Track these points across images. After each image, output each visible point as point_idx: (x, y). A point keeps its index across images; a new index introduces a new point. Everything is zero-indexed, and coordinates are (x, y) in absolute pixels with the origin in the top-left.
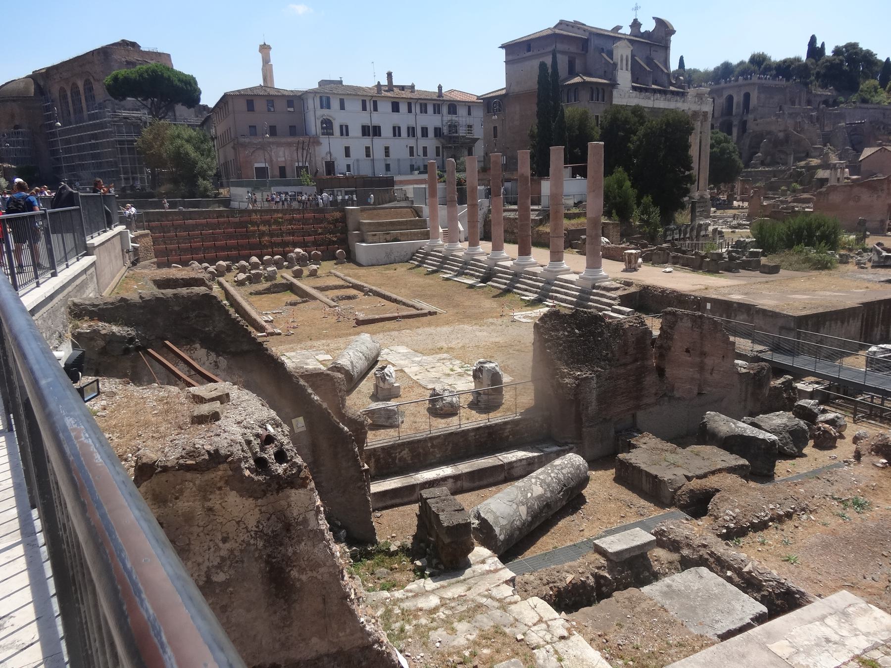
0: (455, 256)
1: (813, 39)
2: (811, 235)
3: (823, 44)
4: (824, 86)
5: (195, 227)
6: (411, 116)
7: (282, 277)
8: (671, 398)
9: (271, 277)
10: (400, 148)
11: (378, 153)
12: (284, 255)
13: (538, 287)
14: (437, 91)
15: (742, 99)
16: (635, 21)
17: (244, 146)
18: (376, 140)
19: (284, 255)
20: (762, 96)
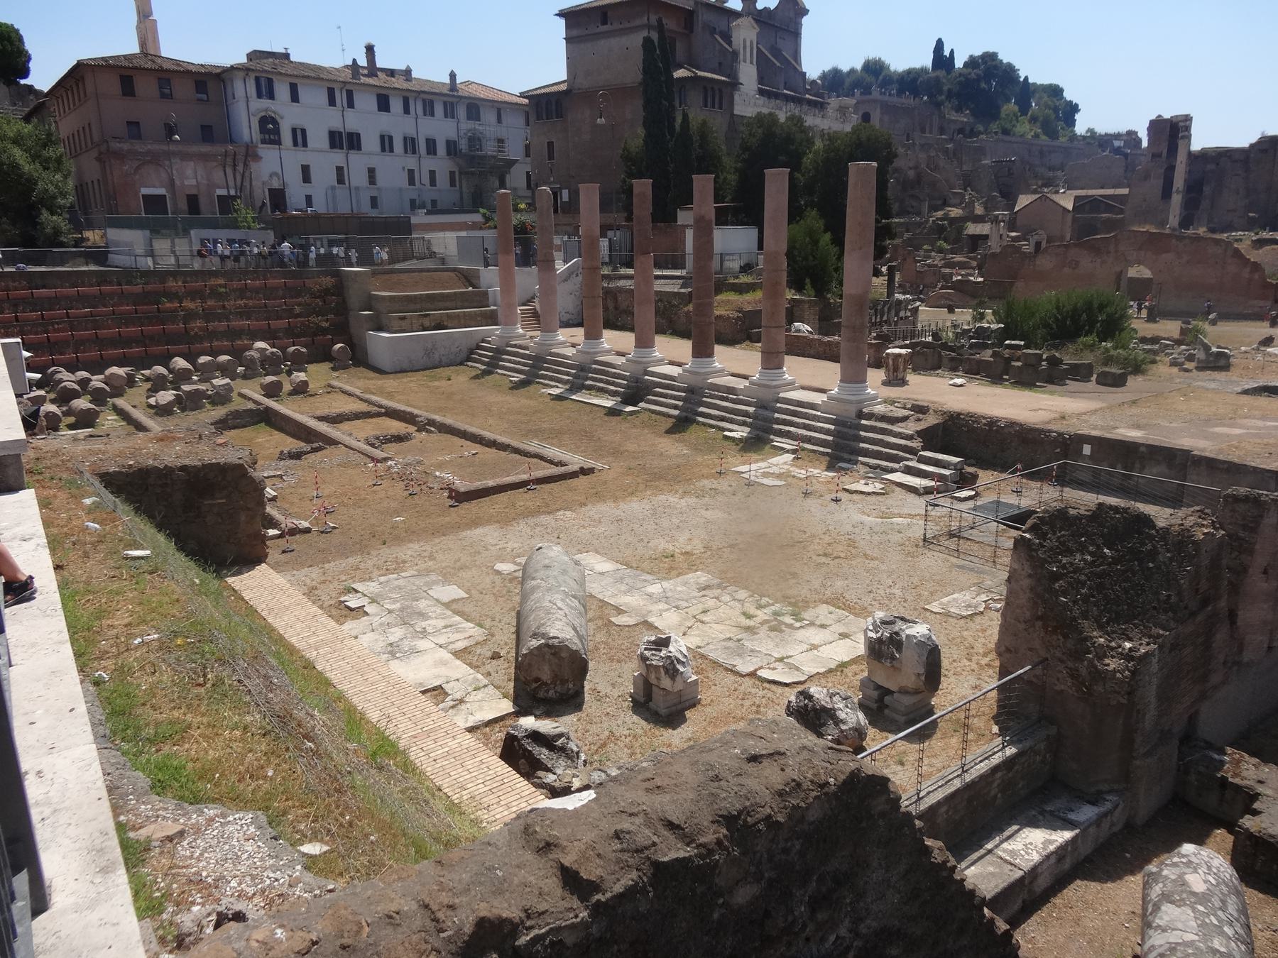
0: (558, 355)
1: (940, 44)
2: (1092, 322)
3: (952, 52)
4: (959, 109)
5: (53, 302)
6: (409, 120)
7: (241, 395)
9: (221, 398)
10: (393, 171)
11: (358, 177)
12: (237, 354)
13: (746, 414)
14: (447, 81)
17: (121, 156)
18: (354, 156)
19: (237, 354)
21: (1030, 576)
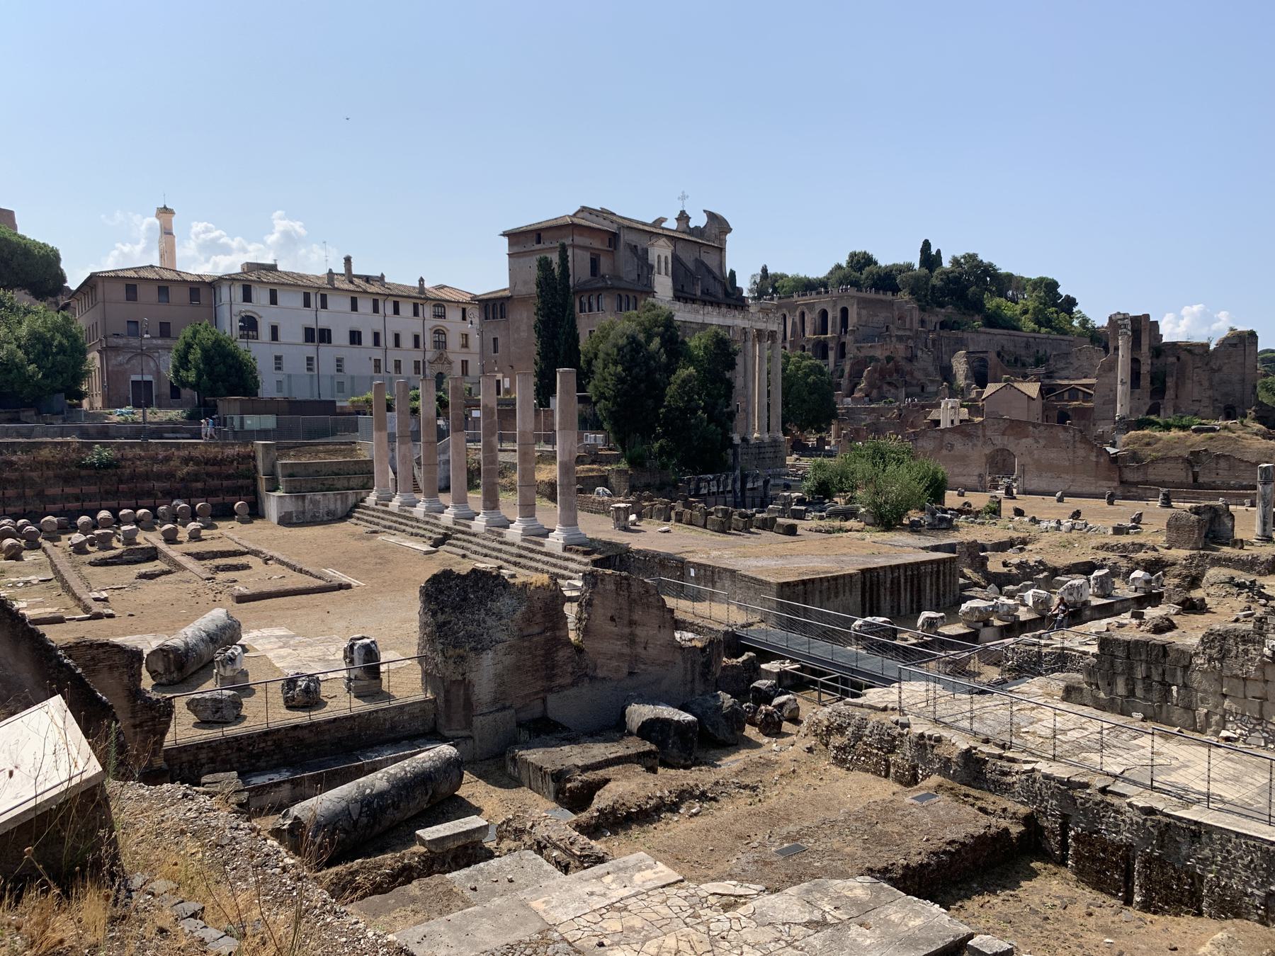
1: (927, 245)
3: (939, 252)
8: (593, 679)
15: (839, 315)
16: (683, 212)
18: (324, 348)
20: (864, 312)
21: (186, 644)
